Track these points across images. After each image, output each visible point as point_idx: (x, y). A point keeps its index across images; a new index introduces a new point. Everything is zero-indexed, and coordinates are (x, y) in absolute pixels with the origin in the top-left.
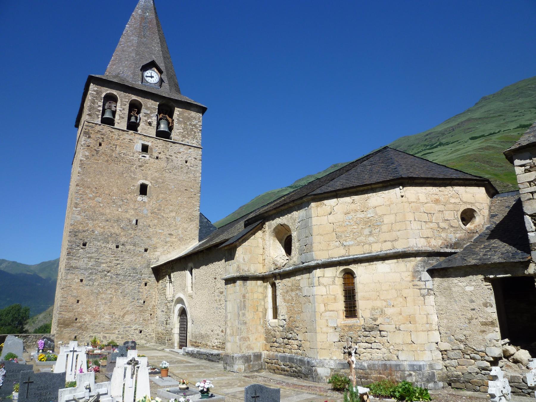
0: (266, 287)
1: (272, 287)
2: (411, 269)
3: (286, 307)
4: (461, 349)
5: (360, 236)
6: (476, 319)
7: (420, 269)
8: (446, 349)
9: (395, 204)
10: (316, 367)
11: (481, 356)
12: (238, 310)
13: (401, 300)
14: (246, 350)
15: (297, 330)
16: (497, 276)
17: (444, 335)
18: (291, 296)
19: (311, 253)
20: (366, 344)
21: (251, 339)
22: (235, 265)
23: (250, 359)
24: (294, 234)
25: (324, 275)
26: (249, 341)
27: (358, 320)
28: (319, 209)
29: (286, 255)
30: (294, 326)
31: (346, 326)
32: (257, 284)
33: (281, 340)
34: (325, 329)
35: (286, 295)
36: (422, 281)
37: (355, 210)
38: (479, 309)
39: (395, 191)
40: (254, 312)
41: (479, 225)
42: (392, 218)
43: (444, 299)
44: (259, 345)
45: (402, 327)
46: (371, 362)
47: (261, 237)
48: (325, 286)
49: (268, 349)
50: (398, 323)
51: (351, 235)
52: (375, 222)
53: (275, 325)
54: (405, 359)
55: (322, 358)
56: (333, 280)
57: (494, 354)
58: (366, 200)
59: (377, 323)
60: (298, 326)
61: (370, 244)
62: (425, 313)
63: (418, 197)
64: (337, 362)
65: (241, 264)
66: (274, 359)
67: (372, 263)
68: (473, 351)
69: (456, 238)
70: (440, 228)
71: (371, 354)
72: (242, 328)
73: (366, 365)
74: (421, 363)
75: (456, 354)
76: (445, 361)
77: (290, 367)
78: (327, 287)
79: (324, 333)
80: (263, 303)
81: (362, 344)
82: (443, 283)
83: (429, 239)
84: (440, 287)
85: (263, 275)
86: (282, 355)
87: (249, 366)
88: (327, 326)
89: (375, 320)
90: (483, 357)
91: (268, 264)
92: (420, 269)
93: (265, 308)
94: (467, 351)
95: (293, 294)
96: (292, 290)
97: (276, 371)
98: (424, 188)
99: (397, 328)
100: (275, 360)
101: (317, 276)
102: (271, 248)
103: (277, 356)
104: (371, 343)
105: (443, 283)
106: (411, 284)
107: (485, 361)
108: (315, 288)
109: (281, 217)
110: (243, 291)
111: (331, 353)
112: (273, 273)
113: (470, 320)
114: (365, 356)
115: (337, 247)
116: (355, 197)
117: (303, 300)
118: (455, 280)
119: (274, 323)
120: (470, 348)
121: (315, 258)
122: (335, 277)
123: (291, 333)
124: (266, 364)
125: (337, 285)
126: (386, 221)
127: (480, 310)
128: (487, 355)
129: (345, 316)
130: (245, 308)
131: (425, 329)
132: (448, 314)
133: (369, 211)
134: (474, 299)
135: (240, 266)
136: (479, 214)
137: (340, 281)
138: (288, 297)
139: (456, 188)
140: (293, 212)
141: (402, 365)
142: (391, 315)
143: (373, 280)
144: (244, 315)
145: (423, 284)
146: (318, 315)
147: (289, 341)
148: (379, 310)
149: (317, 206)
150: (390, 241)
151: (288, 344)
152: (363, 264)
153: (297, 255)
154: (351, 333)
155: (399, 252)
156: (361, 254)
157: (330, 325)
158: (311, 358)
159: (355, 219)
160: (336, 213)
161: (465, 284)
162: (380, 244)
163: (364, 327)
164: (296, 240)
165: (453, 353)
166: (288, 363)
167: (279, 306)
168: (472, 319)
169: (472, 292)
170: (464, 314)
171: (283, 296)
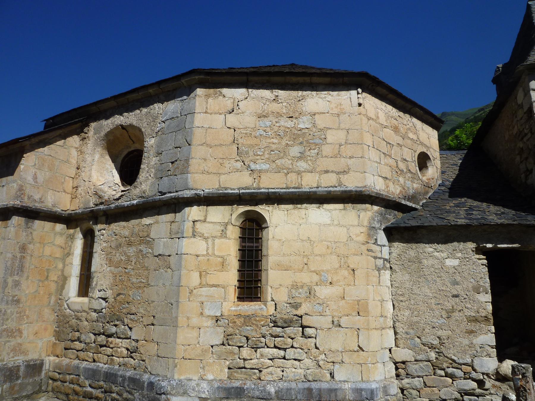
0: (72, 238)
1: (85, 236)
2: (366, 223)
3: (111, 275)
4: (431, 359)
5: (282, 158)
6: (460, 311)
7: (377, 225)
8: (404, 359)
9: (347, 115)
10: (168, 396)
11: (464, 372)
12: (5, 274)
13: (345, 273)
14: (11, 355)
15: (131, 319)
16: (499, 246)
17: (404, 336)
18: (125, 254)
19: (184, 176)
20: (275, 350)
21: (25, 333)
22: (15, 185)
23: (17, 374)
24: (150, 142)
25: (205, 219)
26: (21, 337)
27: (263, 306)
28: (210, 100)
29: (120, 184)
30: (124, 311)
31: (239, 316)
32: (53, 229)
33: (90, 337)
34: (195, 321)
35: (114, 252)
36: (378, 245)
37: (278, 113)
38: (465, 296)
39: (348, 95)
40: (40, 281)
41: (433, 179)
42: (341, 136)
43: (407, 277)
44: (40, 344)
45: (344, 321)
46: (282, 385)
47: (77, 146)
48: (206, 239)
49: (58, 352)
50: (337, 314)
51: (267, 152)
52: (310, 137)
53: (80, 309)
54: (346, 379)
55: (182, 377)
56: (222, 228)
57: (487, 369)
58: (299, 100)
59: (299, 312)
60: (133, 312)
61: (299, 173)
62: (380, 299)
63: (378, 113)
64: (216, 386)
65: (27, 185)
66: (69, 374)
67: (299, 206)
68: (451, 364)
69: (413, 188)
70: (399, 168)
71: (282, 369)
72: (9, 311)
73: (273, 390)
74: (374, 386)
75: (422, 368)
76: (402, 379)
77: (106, 392)
78: (210, 241)
79: (193, 328)
80: (60, 266)
81: (267, 350)
82: (407, 251)
83: (387, 181)
84: (402, 257)
85: (69, 214)
86: (90, 367)
87: (12, 388)
88: (202, 314)
89: (296, 306)
90: (468, 373)
91: (83, 194)
92: (377, 225)
93: (63, 275)
94: (442, 364)
95: (132, 251)
96: (130, 244)
97: (70, 396)
98: (384, 104)
99: (336, 323)
100: (72, 376)
101: (190, 219)
102: (94, 167)
103: (78, 368)
104: (285, 350)
105: (407, 251)
106: (364, 248)
107: (469, 380)
108: (185, 241)
109: (126, 114)
110: (23, 237)
111: (203, 368)
112: (92, 211)
113: (450, 312)
114: (272, 374)
115: (238, 170)
116: (280, 91)
117: (151, 262)
118: (429, 248)
119: (79, 303)
120: (446, 359)
121: (191, 184)
122: (226, 224)
123: (116, 325)
124: (51, 381)
125: (229, 239)
126: (330, 139)
127: (467, 297)
128: (474, 370)
129: (238, 298)
130: (22, 271)
131: (378, 327)
132: (412, 302)
133: (302, 119)
134: (458, 279)
135: (24, 188)
136: (433, 165)
137: (234, 233)
138: (118, 257)
139: (415, 120)
140: (153, 104)
141: (341, 389)
142: (325, 298)
143: (299, 235)
144: (17, 284)
145: (378, 250)
146: (184, 294)
147: (110, 339)
148: (306, 289)
149: (208, 96)
150: (335, 172)
151: (105, 346)
152: (283, 206)
153: (151, 180)
154: (249, 330)
155: (350, 191)
156: (281, 189)
157: (207, 312)
158: (158, 375)
159: (276, 129)
160: (243, 113)
161: (445, 255)
162: (317, 175)
163: (274, 319)
164: (151, 153)
165: (416, 367)
166: (102, 383)
167: (95, 272)
168: (453, 310)
169: (457, 268)
170: (440, 302)
171: (107, 255)
